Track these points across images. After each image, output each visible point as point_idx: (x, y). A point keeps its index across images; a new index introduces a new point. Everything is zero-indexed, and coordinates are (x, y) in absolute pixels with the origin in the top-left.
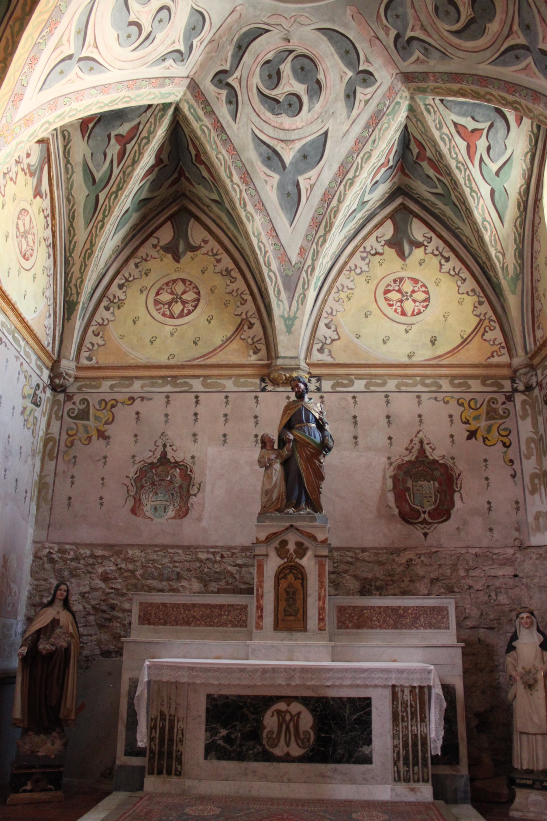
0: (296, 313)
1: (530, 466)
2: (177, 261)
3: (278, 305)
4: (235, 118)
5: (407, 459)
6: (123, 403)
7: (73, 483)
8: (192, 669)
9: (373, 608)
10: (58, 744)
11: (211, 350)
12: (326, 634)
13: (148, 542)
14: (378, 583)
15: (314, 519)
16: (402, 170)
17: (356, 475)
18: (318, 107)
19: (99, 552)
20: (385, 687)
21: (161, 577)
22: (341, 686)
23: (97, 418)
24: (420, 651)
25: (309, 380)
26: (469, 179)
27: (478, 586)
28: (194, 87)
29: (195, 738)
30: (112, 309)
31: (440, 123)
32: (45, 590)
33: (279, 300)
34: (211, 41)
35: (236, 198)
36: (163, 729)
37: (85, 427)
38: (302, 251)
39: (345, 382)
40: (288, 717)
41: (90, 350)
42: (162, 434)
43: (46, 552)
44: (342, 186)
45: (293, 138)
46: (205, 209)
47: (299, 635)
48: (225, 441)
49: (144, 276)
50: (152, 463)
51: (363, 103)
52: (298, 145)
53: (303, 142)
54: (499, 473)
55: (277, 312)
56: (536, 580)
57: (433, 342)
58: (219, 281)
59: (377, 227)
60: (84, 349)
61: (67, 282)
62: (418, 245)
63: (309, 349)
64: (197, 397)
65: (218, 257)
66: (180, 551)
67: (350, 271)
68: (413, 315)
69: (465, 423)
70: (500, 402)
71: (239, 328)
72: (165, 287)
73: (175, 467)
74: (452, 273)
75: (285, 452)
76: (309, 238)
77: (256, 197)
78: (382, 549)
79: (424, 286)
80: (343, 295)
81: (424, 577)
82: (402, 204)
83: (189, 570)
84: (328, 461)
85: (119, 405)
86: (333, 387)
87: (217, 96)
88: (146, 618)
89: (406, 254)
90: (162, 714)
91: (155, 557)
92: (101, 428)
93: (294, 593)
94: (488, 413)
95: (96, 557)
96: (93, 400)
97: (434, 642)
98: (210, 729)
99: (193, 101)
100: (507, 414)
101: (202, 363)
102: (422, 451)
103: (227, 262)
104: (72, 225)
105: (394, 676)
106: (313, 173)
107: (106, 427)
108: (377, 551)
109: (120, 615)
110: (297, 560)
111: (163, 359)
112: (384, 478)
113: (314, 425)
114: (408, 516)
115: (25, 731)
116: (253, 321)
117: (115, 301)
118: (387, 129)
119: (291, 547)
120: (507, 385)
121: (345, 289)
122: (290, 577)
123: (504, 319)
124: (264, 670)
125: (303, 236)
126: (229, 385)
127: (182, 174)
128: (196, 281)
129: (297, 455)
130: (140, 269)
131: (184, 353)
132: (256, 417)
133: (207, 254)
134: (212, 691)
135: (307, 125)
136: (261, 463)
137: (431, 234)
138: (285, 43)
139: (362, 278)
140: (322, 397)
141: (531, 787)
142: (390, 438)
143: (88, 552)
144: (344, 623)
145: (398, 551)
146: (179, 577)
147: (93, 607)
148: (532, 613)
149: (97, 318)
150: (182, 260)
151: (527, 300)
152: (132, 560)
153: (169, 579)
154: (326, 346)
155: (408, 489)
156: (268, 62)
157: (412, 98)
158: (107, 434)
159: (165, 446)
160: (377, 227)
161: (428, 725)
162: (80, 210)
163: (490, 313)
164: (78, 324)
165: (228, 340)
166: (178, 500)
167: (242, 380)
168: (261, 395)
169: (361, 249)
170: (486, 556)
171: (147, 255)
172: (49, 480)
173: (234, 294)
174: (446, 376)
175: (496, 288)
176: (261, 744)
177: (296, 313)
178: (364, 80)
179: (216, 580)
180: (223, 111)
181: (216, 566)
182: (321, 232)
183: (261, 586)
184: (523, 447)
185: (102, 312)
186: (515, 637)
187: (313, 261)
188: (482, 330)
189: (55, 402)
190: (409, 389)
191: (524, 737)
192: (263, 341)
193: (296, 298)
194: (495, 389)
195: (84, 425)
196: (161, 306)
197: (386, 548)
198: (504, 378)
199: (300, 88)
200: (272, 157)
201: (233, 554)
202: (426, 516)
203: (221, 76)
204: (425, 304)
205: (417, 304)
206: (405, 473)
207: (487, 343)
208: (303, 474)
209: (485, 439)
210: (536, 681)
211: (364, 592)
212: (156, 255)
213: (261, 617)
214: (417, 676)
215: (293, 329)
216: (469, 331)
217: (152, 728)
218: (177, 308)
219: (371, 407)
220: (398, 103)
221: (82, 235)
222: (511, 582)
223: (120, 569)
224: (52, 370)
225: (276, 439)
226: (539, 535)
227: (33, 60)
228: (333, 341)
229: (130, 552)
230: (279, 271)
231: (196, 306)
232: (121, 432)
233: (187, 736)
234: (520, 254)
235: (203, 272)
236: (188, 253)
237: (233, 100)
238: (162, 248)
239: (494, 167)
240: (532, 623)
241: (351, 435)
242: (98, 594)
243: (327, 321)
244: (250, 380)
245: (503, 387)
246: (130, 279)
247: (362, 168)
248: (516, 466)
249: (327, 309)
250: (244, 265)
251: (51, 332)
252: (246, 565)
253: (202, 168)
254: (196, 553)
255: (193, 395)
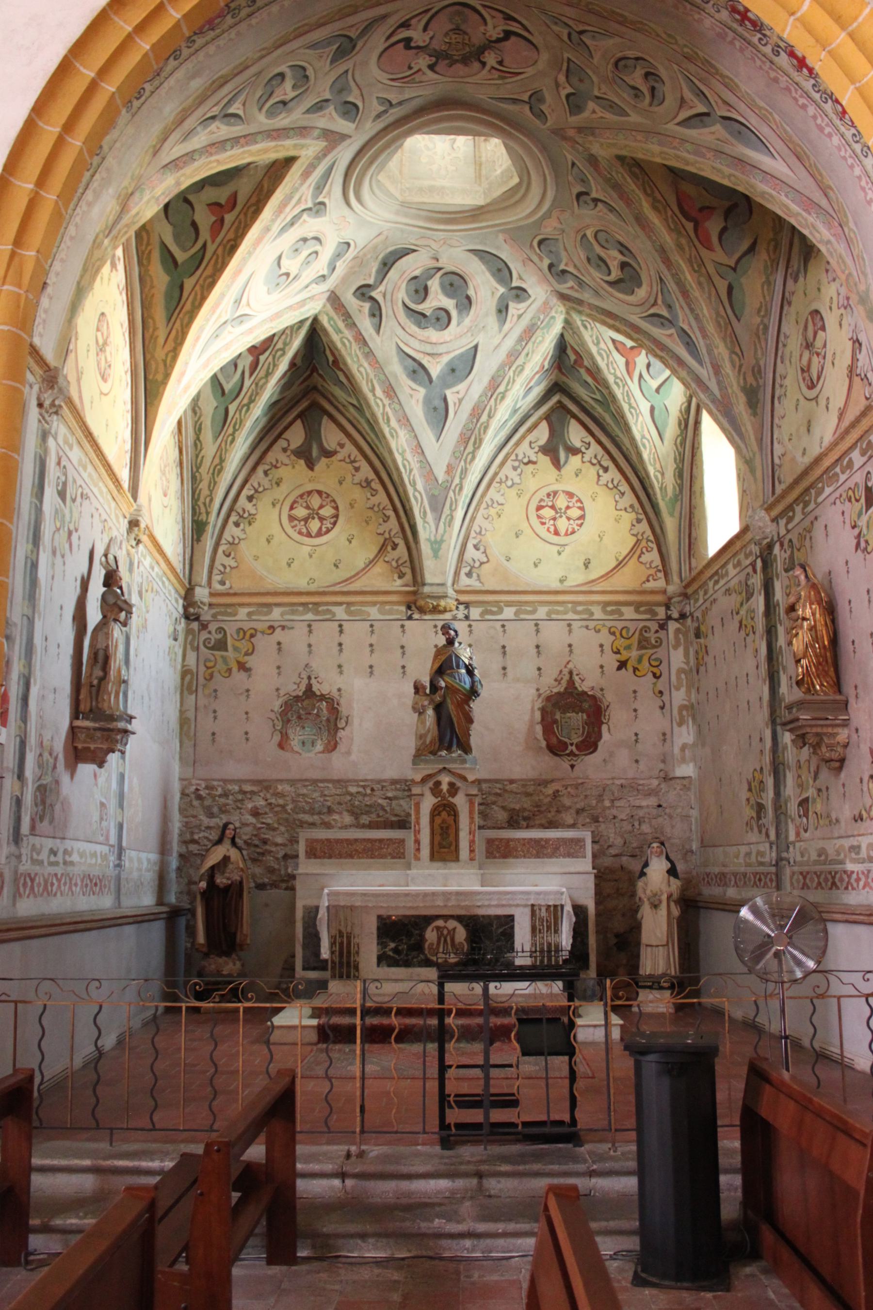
0: (443, 536)
1: (679, 697)
2: (311, 469)
3: (425, 528)
4: (378, 330)
5: (555, 690)
6: (263, 633)
7: (215, 718)
8: (365, 895)
9: (518, 840)
10: (238, 964)
11: (353, 573)
12: (476, 863)
13: (297, 777)
14: (526, 814)
15: (464, 761)
16: (559, 368)
17: (505, 713)
18: (467, 321)
19: (248, 788)
20: (526, 906)
21: (312, 812)
22: (489, 906)
23: (236, 649)
24: (559, 876)
25: (457, 608)
26: (628, 395)
27: (623, 816)
28: (334, 299)
29: (368, 950)
30: (242, 525)
31: (597, 338)
32: (196, 826)
33: (425, 522)
34: (354, 258)
35: (379, 412)
36: (341, 944)
37: (224, 659)
38: (450, 469)
39: (494, 609)
40: (445, 932)
41: (222, 573)
42: (307, 665)
43: (193, 788)
44: (493, 400)
45: (440, 351)
46: (341, 407)
47: (453, 864)
48: (371, 673)
49: (275, 486)
50: (297, 697)
51: (515, 318)
52: (446, 359)
53: (452, 355)
54: (648, 704)
55: (423, 534)
56: (679, 810)
57: (587, 564)
58: (358, 494)
59: (530, 430)
60: (215, 571)
61: (195, 500)
62: (575, 451)
63: (457, 573)
64: (340, 626)
65: (356, 465)
66: (330, 785)
67: (501, 482)
68: (566, 534)
69: (616, 653)
70: (653, 631)
71: (382, 549)
72: (299, 500)
73: (321, 700)
74: (610, 485)
75: (438, 698)
76: (457, 454)
77: (401, 412)
78: (530, 780)
79: (579, 501)
80: (492, 512)
81: (570, 808)
82: (559, 402)
83: (340, 804)
84: (476, 707)
85: (259, 635)
86: (482, 614)
87: (360, 311)
88: (313, 853)
89: (562, 462)
90: (340, 932)
91: (305, 791)
92: (240, 659)
93: (447, 828)
94: (639, 642)
95: (245, 793)
96: (231, 629)
97: (572, 870)
98: (381, 943)
99: (332, 313)
100: (659, 643)
101: (345, 589)
102: (571, 682)
103: (366, 471)
104: (198, 439)
105: (532, 897)
106: (461, 387)
107: (247, 658)
108: (524, 783)
109: (273, 849)
110: (450, 799)
111: (302, 584)
112: (533, 709)
113: (463, 671)
114: (556, 749)
115: (206, 955)
116: (397, 541)
117: (246, 515)
118: (541, 342)
119: (445, 787)
120: (661, 612)
121: (495, 505)
122: (444, 814)
123: (662, 539)
124: (426, 895)
125: (450, 453)
126: (374, 612)
127: (314, 370)
128: (334, 494)
129: (449, 701)
130: (270, 477)
131: (325, 578)
132: (402, 647)
133: (344, 460)
134: (383, 912)
135: (456, 338)
136: (414, 709)
137: (590, 439)
138: (434, 262)
139: (513, 492)
140: (470, 626)
141: (650, 987)
142: (539, 669)
143: (237, 788)
144: (492, 853)
145: (545, 783)
146: (330, 811)
147: (245, 842)
148: (662, 844)
149: (227, 536)
150: (316, 468)
151: (685, 524)
152: (281, 795)
153: (319, 813)
154: (474, 570)
155: (555, 722)
156: (415, 278)
157: (568, 313)
158: (247, 666)
159: (309, 678)
160: (530, 430)
161: (560, 936)
162: (207, 422)
163: (649, 532)
164: (208, 542)
165: (372, 562)
166: (326, 733)
167: (387, 607)
168: (407, 623)
169: (513, 457)
170: (633, 787)
171: (277, 461)
172: (191, 714)
173: (376, 509)
174: (598, 603)
175: (655, 506)
176: (424, 953)
177: (443, 536)
178: (517, 296)
179: (367, 813)
180: (366, 324)
181: (367, 799)
182: (470, 448)
183: (418, 822)
184: (674, 678)
185: (231, 530)
186: (646, 865)
187: (461, 479)
188: (638, 552)
189: (189, 632)
190: (560, 617)
191: (649, 949)
192: (408, 564)
193: (443, 520)
194: (648, 616)
195: (222, 657)
196: (296, 522)
197: (533, 780)
198: (658, 604)
199: (449, 304)
200: (418, 371)
201: (383, 787)
202: (574, 748)
203: (364, 290)
204: (579, 522)
205: (572, 522)
206: (554, 705)
207: (643, 567)
208: (455, 720)
209: (635, 669)
210: (660, 902)
211: (513, 823)
212: (287, 461)
213: (418, 850)
214: (552, 897)
215: (440, 553)
216: (625, 552)
217: (332, 944)
218: (315, 525)
219: (521, 637)
220: (553, 317)
221: (210, 449)
222: (654, 812)
223: (270, 804)
224: (185, 598)
225: (428, 685)
226: (684, 766)
227: (197, 339)
228: (482, 563)
229: (280, 788)
230: (425, 491)
231: (334, 524)
232: (262, 662)
233: (362, 950)
234: (679, 474)
235: (340, 483)
236: (323, 459)
237: (376, 313)
238: (293, 452)
239: (655, 384)
240: (662, 852)
241: (500, 666)
242: (248, 829)
243: (475, 542)
244: (396, 607)
245: (656, 614)
246: (261, 489)
247: (514, 381)
248: (666, 698)
249: (476, 528)
250: (385, 477)
251: (181, 558)
252: (396, 798)
253: (340, 374)
254: (346, 787)
255: (337, 623)
